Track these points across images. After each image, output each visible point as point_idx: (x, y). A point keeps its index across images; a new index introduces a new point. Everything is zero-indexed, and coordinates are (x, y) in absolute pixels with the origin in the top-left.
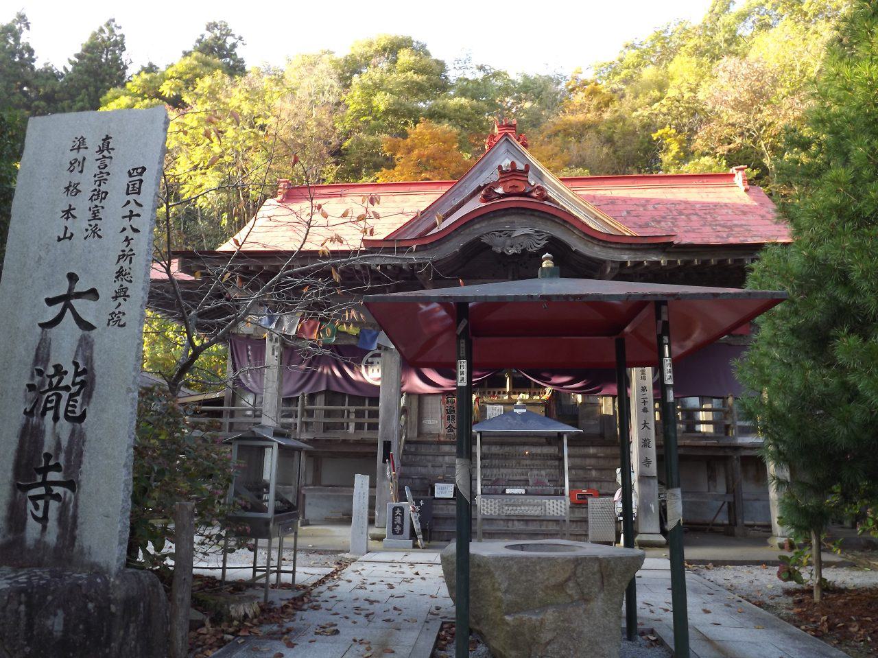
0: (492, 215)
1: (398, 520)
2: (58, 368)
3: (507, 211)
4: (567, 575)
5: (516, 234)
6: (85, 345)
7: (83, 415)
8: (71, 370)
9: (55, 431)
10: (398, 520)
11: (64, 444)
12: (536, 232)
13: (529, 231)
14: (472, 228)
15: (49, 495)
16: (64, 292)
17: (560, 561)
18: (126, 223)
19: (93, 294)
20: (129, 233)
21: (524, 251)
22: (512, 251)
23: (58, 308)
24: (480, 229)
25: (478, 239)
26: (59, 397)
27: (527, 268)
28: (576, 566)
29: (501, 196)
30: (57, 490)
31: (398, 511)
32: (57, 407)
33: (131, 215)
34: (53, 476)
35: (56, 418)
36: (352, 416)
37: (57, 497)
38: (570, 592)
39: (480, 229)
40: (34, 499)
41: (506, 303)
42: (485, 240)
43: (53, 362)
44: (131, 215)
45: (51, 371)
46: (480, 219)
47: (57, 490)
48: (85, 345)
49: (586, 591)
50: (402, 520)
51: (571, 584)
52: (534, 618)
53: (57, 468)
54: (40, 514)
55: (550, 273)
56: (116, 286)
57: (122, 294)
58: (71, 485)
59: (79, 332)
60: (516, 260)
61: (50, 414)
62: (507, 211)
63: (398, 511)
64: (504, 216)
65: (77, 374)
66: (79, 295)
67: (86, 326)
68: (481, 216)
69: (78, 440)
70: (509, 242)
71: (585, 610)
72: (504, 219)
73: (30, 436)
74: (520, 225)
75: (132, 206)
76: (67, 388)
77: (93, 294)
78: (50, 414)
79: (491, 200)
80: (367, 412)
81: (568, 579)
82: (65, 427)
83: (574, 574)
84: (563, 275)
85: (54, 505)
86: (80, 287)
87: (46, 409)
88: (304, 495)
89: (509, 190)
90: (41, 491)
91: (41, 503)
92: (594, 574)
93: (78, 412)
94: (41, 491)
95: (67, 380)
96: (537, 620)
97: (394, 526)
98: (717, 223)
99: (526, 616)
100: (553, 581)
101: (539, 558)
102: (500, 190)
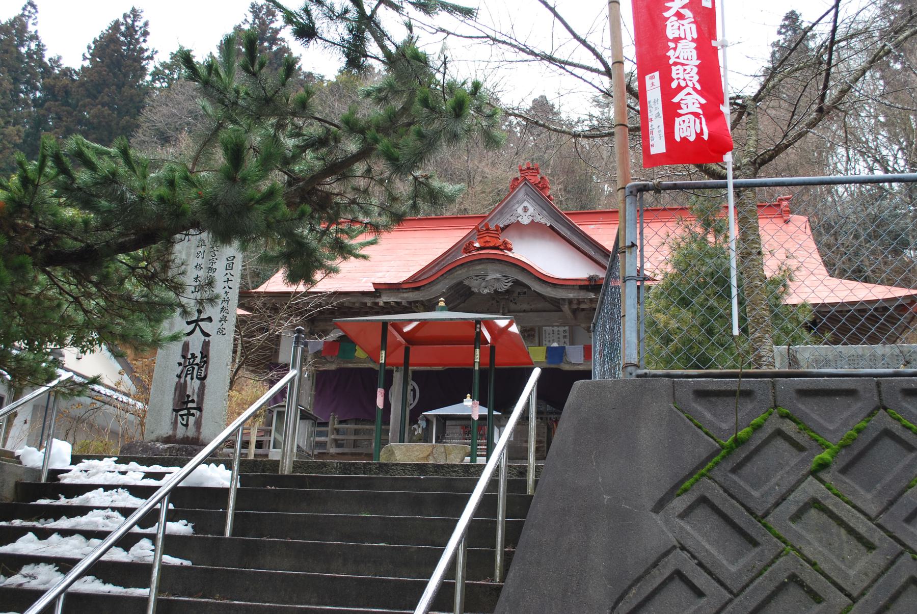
2: (193, 355)
5: (488, 278)
6: (206, 345)
7: (205, 377)
8: (199, 356)
9: (193, 385)
11: (196, 390)
13: (498, 276)
15: (189, 414)
16: (195, 318)
18: (226, 284)
19: (210, 319)
20: (227, 289)
21: (496, 291)
22: (486, 291)
23: (192, 326)
24: (461, 274)
25: (461, 283)
26: (194, 368)
30: (192, 411)
32: (192, 373)
33: (228, 280)
34: (190, 405)
35: (192, 379)
37: (193, 415)
39: (461, 274)
40: (182, 416)
42: (466, 283)
43: (191, 352)
44: (228, 280)
45: (190, 356)
47: (192, 411)
48: (206, 345)
53: (193, 401)
54: (184, 423)
55: (442, 309)
56: (221, 315)
57: (224, 319)
58: (200, 409)
59: (203, 338)
61: (189, 376)
62: (480, 261)
64: (480, 264)
65: (202, 358)
66: (203, 320)
67: (206, 335)
68: (462, 265)
69: (202, 388)
70: (483, 284)
73: (181, 388)
75: (229, 276)
76: (197, 364)
77: (210, 319)
78: (189, 376)
79: (470, 252)
81: (429, 455)
82: (196, 383)
84: (450, 310)
85: (191, 418)
86: (203, 316)
87: (187, 375)
89: (483, 245)
90: (185, 412)
91: (185, 417)
93: (203, 375)
94: (185, 412)
95: (198, 361)
100: (421, 456)
102: (477, 245)
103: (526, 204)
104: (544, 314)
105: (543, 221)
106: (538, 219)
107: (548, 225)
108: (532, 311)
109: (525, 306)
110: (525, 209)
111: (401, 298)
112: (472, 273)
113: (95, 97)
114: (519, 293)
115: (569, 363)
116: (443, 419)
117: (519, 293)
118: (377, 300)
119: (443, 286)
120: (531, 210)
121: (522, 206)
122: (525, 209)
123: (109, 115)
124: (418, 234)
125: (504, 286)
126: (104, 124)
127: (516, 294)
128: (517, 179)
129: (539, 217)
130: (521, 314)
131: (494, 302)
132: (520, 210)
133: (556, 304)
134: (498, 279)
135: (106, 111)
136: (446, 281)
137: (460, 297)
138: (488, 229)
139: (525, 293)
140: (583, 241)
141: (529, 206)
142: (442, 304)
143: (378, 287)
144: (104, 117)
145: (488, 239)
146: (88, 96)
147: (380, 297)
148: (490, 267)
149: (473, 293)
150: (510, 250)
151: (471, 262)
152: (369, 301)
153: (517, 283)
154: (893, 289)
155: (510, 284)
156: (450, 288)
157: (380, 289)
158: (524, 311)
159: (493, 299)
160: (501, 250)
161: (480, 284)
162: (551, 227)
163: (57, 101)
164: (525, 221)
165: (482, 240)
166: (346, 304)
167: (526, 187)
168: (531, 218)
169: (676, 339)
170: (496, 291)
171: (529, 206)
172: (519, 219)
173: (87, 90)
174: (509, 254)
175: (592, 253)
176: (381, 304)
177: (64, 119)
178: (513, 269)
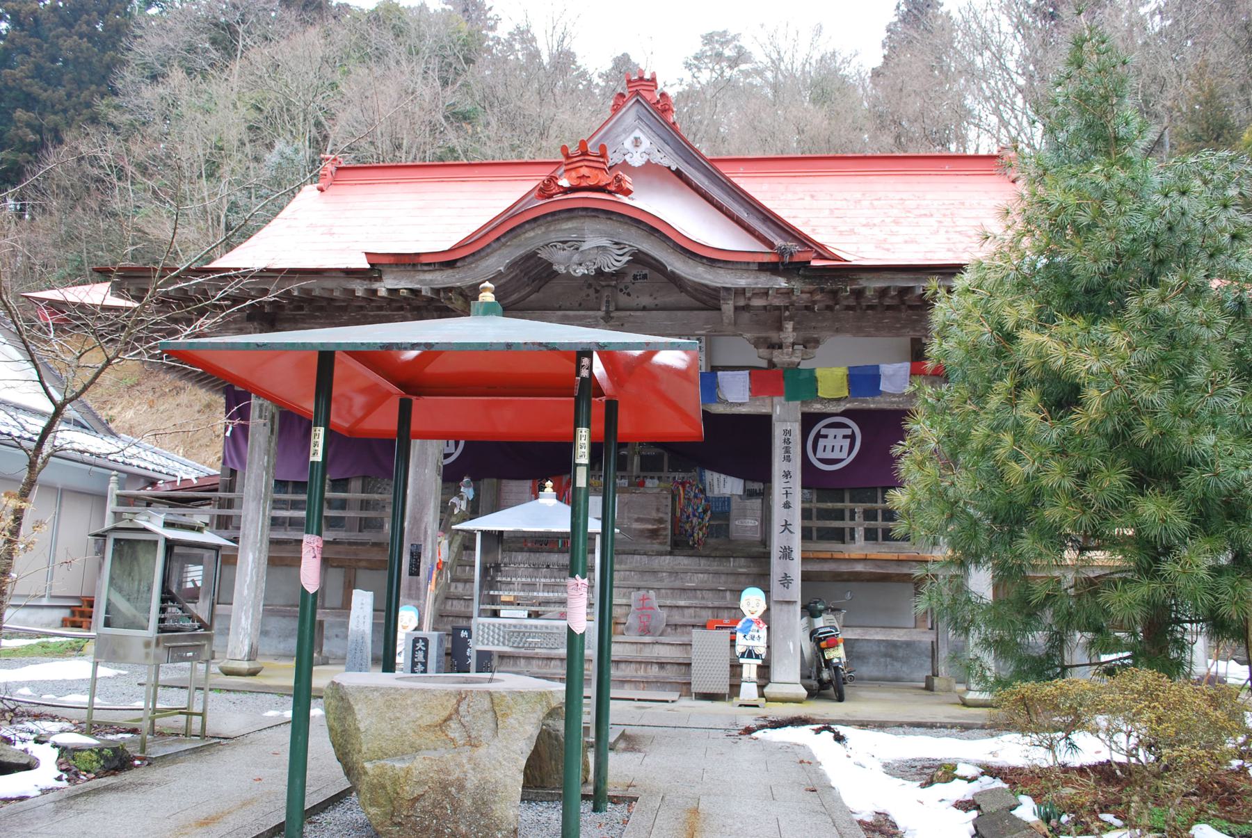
0: (549, 219)
1: (420, 656)
3: (571, 213)
4: (445, 714)
5: (585, 246)
10: (420, 656)
12: (616, 243)
13: (604, 242)
14: (523, 237)
17: (436, 693)
21: (599, 272)
22: (581, 271)
24: (532, 239)
25: (533, 255)
27: (629, 294)
28: (459, 702)
29: (566, 191)
31: (420, 644)
36: (859, 518)
38: (452, 735)
39: (532, 239)
41: (439, 353)
42: (543, 255)
46: (533, 225)
49: (474, 734)
50: (426, 657)
51: (453, 724)
52: (398, 765)
55: (488, 310)
60: (614, 283)
62: (571, 213)
63: (420, 644)
68: (535, 220)
70: (576, 258)
71: (470, 759)
72: (569, 225)
74: (592, 232)
79: (551, 196)
80: (880, 512)
83: (457, 711)
88: (321, 623)
89: (575, 183)
92: (485, 712)
96: (401, 769)
97: (414, 664)
98: (958, 229)
99: (388, 763)
100: (427, 720)
101: (411, 689)
102: (564, 183)
103: (637, 133)
104: (679, 313)
105: (666, 162)
106: (657, 158)
107: (673, 168)
108: (657, 308)
109: (645, 300)
110: (637, 142)
111: (421, 282)
112: (553, 237)
113: (70, 26)
114: (635, 277)
115: (725, 402)
116: (494, 539)
117: (635, 277)
118: (376, 285)
119: (498, 262)
120: (646, 143)
121: (632, 138)
122: (637, 142)
123: (88, 49)
124: (466, 186)
125: (613, 262)
126: (82, 60)
127: (629, 279)
128: (622, 95)
129: (659, 155)
130: (638, 313)
131: (591, 292)
132: (628, 144)
133: (709, 299)
134: (604, 248)
135: (85, 43)
136: (505, 251)
137: (530, 288)
138: (585, 153)
139: (645, 277)
140: (729, 195)
141: (643, 137)
142: (488, 297)
143: (375, 260)
144: (82, 51)
145: (584, 171)
146: (63, 25)
147: (380, 279)
148: (589, 225)
149: (555, 274)
150: (627, 192)
151: (553, 214)
152: (359, 288)
153: (639, 258)
154: (60, 298)
155: (626, 258)
156: (513, 265)
157: (379, 265)
158: (644, 309)
159: (590, 286)
160: (610, 193)
161: (570, 258)
162: (678, 173)
163: (23, 30)
164: (637, 160)
165: (574, 174)
166: (317, 293)
167: (637, 107)
168: (646, 157)
169: (1094, 396)
170: (599, 272)
171: (643, 137)
172: (627, 158)
173: (61, 17)
174: (625, 200)
175: (743, 214)
176: (382, 292)
177: (33, 53)
178: (633, 230)
